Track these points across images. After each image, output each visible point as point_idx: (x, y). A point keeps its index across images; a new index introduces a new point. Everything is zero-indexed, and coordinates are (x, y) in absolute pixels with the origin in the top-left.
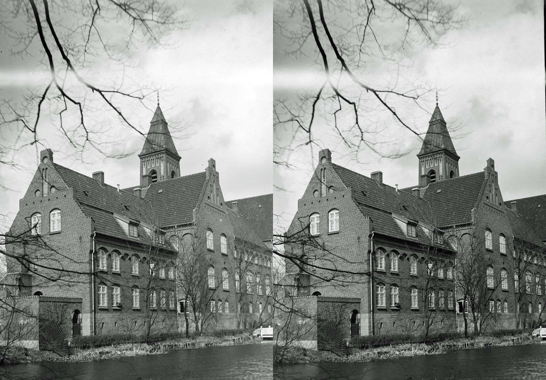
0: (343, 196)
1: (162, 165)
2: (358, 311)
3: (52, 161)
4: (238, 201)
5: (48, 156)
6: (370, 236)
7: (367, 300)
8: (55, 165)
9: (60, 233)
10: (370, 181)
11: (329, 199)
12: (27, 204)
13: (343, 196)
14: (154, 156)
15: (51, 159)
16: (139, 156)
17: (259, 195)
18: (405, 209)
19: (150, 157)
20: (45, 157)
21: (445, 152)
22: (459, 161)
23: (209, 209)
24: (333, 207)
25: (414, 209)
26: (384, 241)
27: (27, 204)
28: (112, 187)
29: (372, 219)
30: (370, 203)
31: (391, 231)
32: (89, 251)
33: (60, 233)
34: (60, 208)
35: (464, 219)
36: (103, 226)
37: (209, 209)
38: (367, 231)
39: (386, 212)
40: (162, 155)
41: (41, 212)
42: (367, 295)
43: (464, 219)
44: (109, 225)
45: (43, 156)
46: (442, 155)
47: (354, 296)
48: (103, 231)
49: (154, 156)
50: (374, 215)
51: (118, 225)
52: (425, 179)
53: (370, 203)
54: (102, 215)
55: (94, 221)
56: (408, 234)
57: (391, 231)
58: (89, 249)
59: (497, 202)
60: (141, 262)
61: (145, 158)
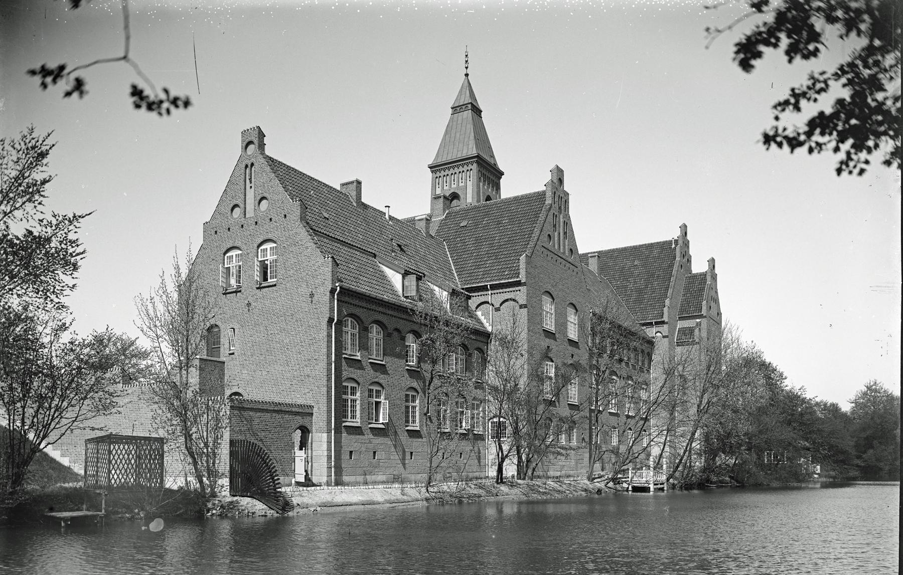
0: (285, 216)
1: (469, 184)
2: (308, 427)
3: (264, 150)
4: (599, 252)
5: (256, 141)
6: (332, 291)
7: (325, 409)
8: (271, 161)
9: (275, 285)
10: (338, 194)
11: (259, 222)
12: (216, 232)
13: (285, 216)
14: (456, 168)
15: (262, 146)
16: (430, 168)
17: (635, 244)
18: (402, 249)
19: (449, 169)
20: (250, 143)
21: (477, 162)
22: (501, 180)
23: (549, 258)
24: (265, 238)
25: (417, 251)
26: (360, 304)
27: (216, 232)
28: (375, 209)
29: (338, 262)
30: (336, 232)
31: (372, 285)
32: (327, 320)
33: (275, 285)
34: (274, 239)
35: (506, 273)
36: (354, 275)
37: (549, 258)
38: (326, 282)
39: (365, 252)
40: (470, 167)
41: (243, 247)
42: (324, 400)
43: (506, 273)
44: (366, 275)
45: (247, 141)
46: (472, 167)
47: (300, 401)
48: (355, 284)
49: (456, 168)
50: (342, 255)
51: (384, 277)
52: (440, 203)
53: (336, 232)
54: (355, 256)
55: (336, 263)
56: (403, 295)
57: (372, 285)
58: (328, 316)
59: (567, 247)
60: (388, 335)
61: (440, 171)
